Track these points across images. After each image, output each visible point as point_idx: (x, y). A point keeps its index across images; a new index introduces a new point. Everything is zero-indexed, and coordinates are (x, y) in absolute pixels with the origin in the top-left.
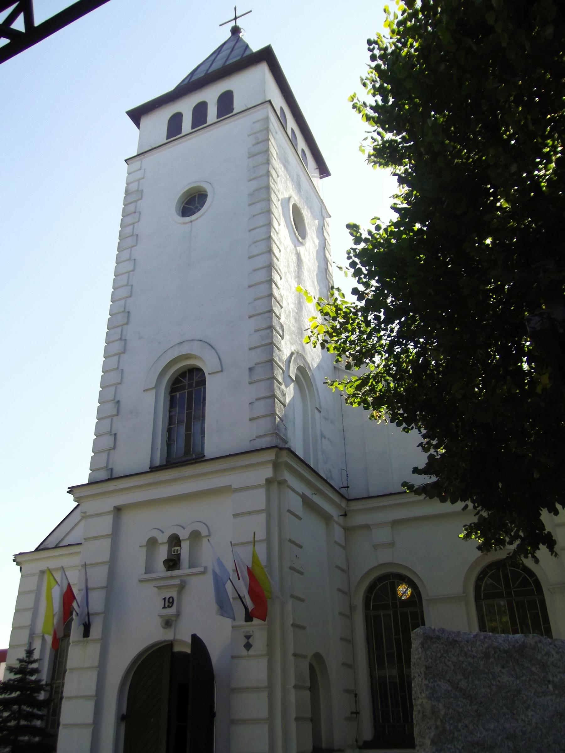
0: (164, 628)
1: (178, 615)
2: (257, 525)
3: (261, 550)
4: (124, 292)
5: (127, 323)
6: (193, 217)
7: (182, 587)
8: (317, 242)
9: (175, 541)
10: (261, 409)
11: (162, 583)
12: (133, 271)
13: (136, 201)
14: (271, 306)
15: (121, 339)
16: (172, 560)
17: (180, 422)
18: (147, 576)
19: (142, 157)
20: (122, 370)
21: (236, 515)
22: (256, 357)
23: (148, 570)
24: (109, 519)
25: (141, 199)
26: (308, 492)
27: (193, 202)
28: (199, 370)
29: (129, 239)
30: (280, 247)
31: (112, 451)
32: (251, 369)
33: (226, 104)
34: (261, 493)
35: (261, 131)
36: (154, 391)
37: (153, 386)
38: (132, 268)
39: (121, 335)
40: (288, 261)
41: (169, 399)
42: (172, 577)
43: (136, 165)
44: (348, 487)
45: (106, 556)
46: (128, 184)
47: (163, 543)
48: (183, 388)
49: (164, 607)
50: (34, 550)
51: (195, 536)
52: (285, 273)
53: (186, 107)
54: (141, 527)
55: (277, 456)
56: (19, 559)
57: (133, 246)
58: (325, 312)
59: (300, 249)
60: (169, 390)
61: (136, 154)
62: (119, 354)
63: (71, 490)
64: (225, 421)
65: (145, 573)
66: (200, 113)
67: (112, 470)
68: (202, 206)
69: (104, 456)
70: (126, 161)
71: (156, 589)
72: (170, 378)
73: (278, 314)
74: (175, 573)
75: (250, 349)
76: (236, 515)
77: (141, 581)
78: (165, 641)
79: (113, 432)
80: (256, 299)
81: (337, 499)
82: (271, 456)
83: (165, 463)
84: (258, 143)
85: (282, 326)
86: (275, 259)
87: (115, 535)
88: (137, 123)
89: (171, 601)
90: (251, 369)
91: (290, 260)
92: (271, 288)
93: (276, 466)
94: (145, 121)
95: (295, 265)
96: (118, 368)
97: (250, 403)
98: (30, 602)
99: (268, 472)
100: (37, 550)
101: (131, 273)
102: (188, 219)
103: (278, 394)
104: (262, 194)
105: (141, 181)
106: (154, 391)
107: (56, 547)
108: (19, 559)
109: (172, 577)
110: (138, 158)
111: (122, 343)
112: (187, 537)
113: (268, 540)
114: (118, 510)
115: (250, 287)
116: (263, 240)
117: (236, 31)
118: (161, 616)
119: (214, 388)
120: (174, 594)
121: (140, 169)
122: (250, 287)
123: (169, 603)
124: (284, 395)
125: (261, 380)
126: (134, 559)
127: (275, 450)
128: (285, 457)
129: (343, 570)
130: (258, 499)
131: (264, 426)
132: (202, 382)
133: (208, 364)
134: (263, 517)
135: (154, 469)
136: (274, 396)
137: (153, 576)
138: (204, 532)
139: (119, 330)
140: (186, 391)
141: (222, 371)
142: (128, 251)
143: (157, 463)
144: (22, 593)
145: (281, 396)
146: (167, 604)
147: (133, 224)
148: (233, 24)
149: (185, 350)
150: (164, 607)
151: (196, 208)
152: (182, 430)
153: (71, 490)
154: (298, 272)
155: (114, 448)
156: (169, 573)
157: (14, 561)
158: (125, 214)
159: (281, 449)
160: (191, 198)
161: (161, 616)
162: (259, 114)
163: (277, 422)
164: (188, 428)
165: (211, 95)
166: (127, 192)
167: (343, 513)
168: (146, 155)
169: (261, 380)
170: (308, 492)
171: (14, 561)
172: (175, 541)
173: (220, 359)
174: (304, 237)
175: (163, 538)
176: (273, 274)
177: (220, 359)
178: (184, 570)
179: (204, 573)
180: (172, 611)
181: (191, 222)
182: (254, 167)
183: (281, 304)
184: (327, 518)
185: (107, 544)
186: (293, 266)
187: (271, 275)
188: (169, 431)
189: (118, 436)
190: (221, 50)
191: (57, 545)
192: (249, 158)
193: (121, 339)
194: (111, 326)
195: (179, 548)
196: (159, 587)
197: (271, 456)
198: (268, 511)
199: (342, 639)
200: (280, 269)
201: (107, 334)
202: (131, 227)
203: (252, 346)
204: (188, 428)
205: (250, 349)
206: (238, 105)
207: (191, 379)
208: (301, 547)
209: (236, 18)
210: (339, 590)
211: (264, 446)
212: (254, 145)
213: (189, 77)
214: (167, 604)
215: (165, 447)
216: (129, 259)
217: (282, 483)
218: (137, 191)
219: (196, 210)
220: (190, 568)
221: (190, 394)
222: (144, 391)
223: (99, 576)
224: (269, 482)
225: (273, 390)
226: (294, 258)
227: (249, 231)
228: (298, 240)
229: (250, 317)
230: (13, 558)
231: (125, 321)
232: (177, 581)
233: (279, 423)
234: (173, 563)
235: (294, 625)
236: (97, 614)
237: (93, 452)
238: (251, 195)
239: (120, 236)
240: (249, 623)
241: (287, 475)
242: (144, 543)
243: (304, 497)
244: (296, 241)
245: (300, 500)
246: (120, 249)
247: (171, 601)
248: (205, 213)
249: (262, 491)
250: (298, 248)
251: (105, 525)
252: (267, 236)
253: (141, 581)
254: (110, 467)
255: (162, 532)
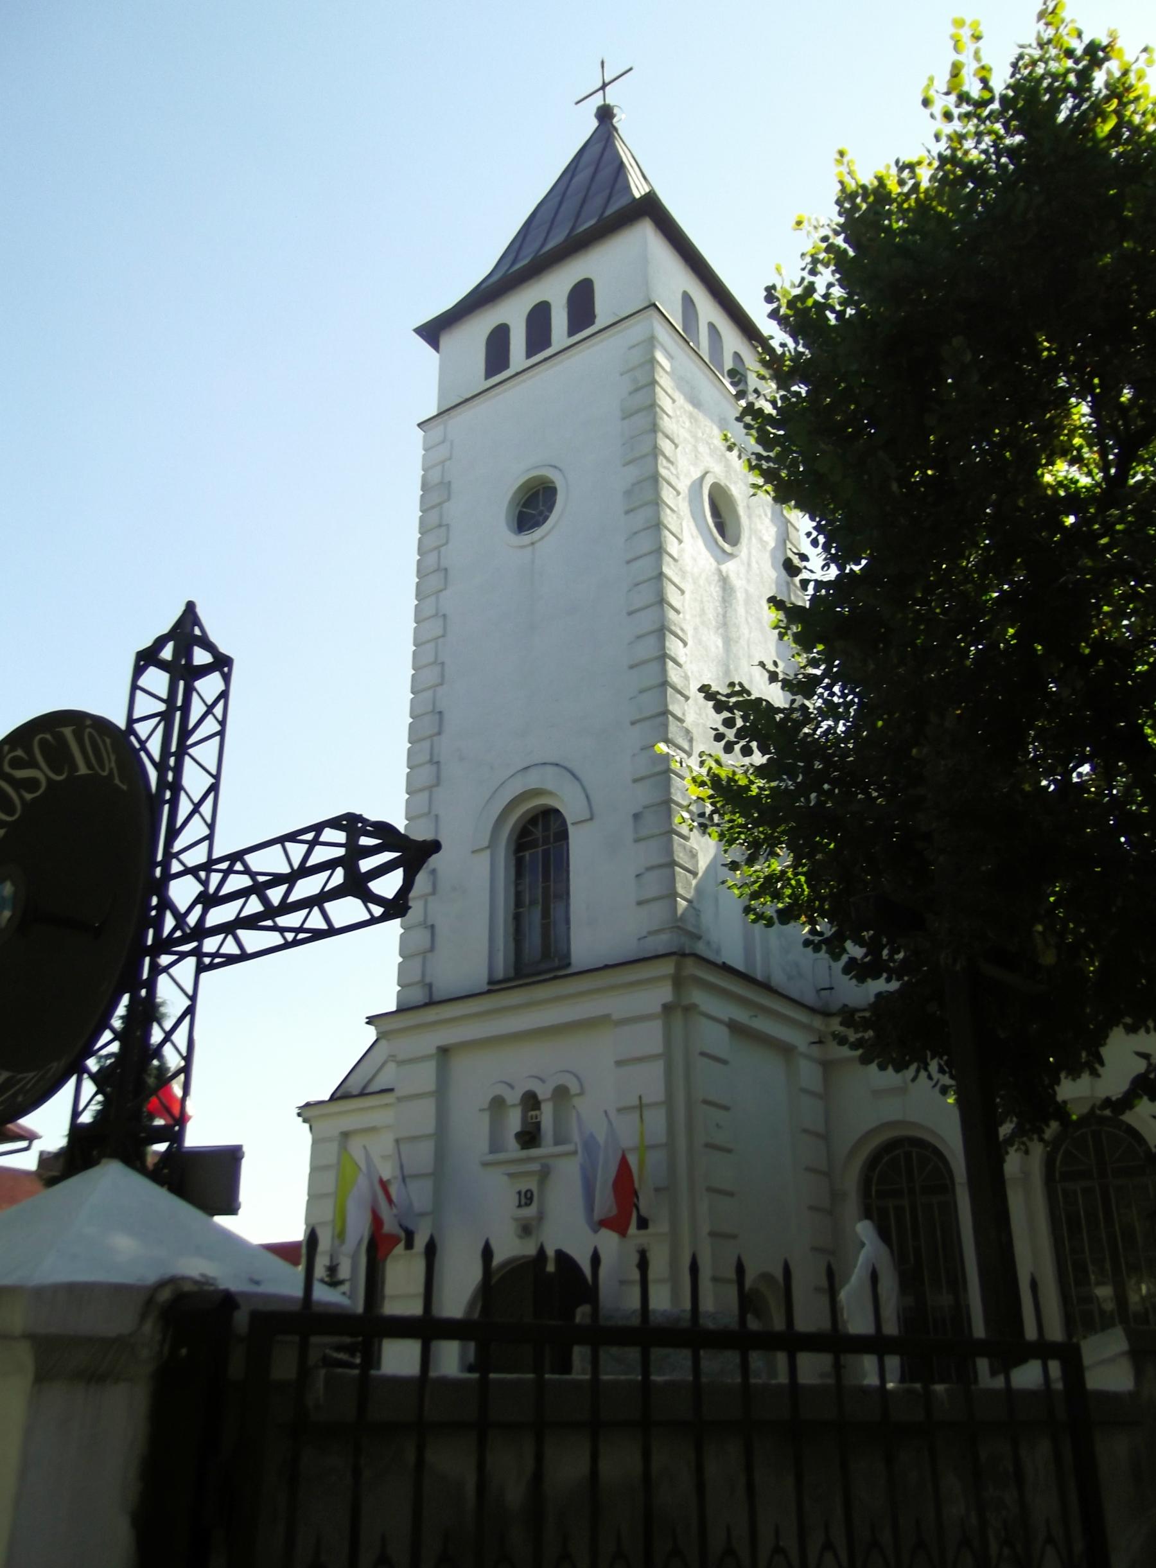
0: (520, 1237)
1: (541, 1217)
2: (650, 1081)
3: (657, 1121)
4: (431, 676)
5: (439, 733)
6: (539, 533)
7: (544, 1174)
8: (773, 530)
9: (531, 1101)
10: (653, 885)
11: (513, 1169)
12: (443, 636)
13: (440, 504)
14: (666, 705)
15: (431, 761)
16: (528, 1133)
17: (533, 903)
18: (491, 1158)
19: (445, 417)
20: (437, 816)
21: (619, 1063)
22: (644, 795)
23: (495, 1146)
24: (430, 1067)
25: (448, 499)
26: (741, 1015)
27: (533, 505)
28: (557, 811)
29: (433, 576)
30: (682, 586)
31: (429, 955)
32: (636, 816)
33: (582, 301)
34: (655, 1028)
35: (641, 365)
36: (488, 852)
37: (486, 844)
38: (440, 633)
39: (431, 754)
40: (702, 602)
41: (513, 862)
42: (530, 1159)
43: (437, 432)
44: (831, 989)
45: (429, 1126)
46: (425, 469)
47: (514, 1106)
48: (533, 844)
49: (520, 1206)
50: (327, 1098)
51: (561, 1093)
52: (696, 629)
53: (513, 312)
54: (480, 1079)
55: (679, 967)
56: (307, 1111)
57: (441, 591)
58: (699, 780)
59: (729, 567)
60: (513, 847)
61: (435, 413)
62: (430, 788)
63: (371, 1020)
64: (602, 907)
65: (491, 1152)
66: (539, 318)
67: (430, 986)
68: (550, 508)
69: (417, 962)
70: (419, 425)
71: (505, 1178)
72: (512, 830)
73: (680, 715)
74: (534, 1152)
75: (635, 781)
76: (619, 1063)
77: (485, 1164)
78: (524, 1257)
79: (429, 923)
80: (641, 692)
81: (802, 1016)
82: (667, 968)
83: (512, 973)
84: (637, 390)
85: (688, 732)
86: (671, 614)
87: (441, 1092)
88: (434, 342)
89: (529, 1195)
90: (636, 816)
91: (705, 599)
92: (664, 671)
93: (678, 982)
94: (445, 340)
95: (718, 604)
96: (429, 812)
97: (637, 876)
98: (329, 1182)
99: (665, 993)
100: (333, 1098)
101: (441, 640)
102: (525, 538)
103: (680, 856)
104: (645, 493)
105: (448, 463)
106: (488, 852)
107: (362, 1094)
108: (307, 1111)
109: (530, 1159)
110: (439, 420)
111: (434, 768)
112: (549, 1095)
113: (669, 1102)
114: (444, 1052)
115: (632, 667)
116: (650, 579)
117: (605, 114)
118: (516, 1220)
119: (582, 846)
120: (533, 1185)
121: (443, 442)
122: (632, 667)
123: (526, 1199)
124: (693, 855)
125: (653, 837)
126: (472, 1130)
127: (674, 958)
128: (692, 968)
129: (817, 1135)
130: (651, 1037)
131: (657, 914)
132: (563, 835)
133: (570, 806)
134: (658, 1067)
135: (495, 985)
136: (673, 863)
137: (501, 1156)
138: (574, 1088)
139: (426, 745)
140: (540, 849)
141: (591, 819)
142: (433, 598)
143: (500, 974)
144: (316, 1169)
145: (686, 858)
146: (523, 1201)
147: (438, 548)
148: (597, 101)
149: (533, 781)
150: (520, 1206)
151: (541, 513)
152: (535, 917)
153: (371, 1020)
154: (724, 616)
155: (432, 948)
156: (524, 1153)
157: (299, 1115)
158: (424, 529)
159: (684, 955)
160: (533, 495)
161: (516, 1220)
162: (634, 332)
163: (680, 911)
164: (546, 914)
165: (554, 289)
166: (425, 486)
167: (816, 1040)
168: (453, 413)
169: (653, 837)
170: (741, 1015)
171: (299, 1115)
172: (531, 1101)
173: (587, 797)
174: (735, 542)
175: (513, 1097)
176: (667, 644)
177: (587, 797)
178: (547, 1148)
179: (575, 1153)
180: (530, 1211)
181: (533, 544)
182: (632, 438)
183: (686, 693)
184: (786, 1050)
185: (429, 1106)
186: (712, 609)
187: (663, 647)
188: (517, 918)
189: (438, 930)
190: (576, 167)
191: (365, 1087)
192: (624, 419)
193: (431, 761)
194: (414, 737)
195: (537, 1112)
196: (510, 1175)
197: (667, 968)
198: (667, 1056)
199: (815, 1249)
200: (682, 630)
201: (410, 752)
202: (435, 553)
203: (638, 776)
204: (546, 914)
205: (635, 781)
206: (604, 309)
207: (546, 828)
208: (726, 1108)
209: (604, 86)
210: (809, 1169)
211: (661, 951)
212: (630, 393)
213: (520, 238)
214: (523, 1201)
215: (512, 945)
216: (436, 615)
217: (689, 1009)
218: (441, 483)
219: (541, 519)
220: (557, 1142)
221: (546, 854)
222: (473, 852)
223: (422, 1156)
224: (667, 1009)
225: (669, 851)
226: (715, 590)
227: (628, 562)
228: (724, 551)
229: (633, 723)
230: (297, 1111)
231: (436, 730)
232: (535, 1167)
233: (686, 909)
234: (530, 1137)
235: (713, 1234)
236: (422, 1215)
237: (401, 955)
238: (628, 493)
239: (418, 571)
240: (642, 1232)
241: (698, 997)
242: (486, 1106)
243: (735, 1028)
244: (719, 553)
245: (724, 1031)
246: (420, 595)
247: (529, 1195)
248: (553, 528)
249: (657, 1026)
250: (724, 568)
251: (425, 1076)
252: (655, 573)
253: (485, 1164)
254: (428, 980)
255: (512, 1087)
